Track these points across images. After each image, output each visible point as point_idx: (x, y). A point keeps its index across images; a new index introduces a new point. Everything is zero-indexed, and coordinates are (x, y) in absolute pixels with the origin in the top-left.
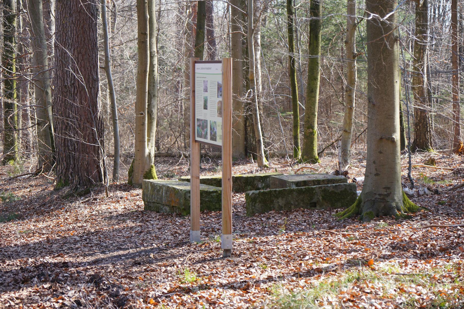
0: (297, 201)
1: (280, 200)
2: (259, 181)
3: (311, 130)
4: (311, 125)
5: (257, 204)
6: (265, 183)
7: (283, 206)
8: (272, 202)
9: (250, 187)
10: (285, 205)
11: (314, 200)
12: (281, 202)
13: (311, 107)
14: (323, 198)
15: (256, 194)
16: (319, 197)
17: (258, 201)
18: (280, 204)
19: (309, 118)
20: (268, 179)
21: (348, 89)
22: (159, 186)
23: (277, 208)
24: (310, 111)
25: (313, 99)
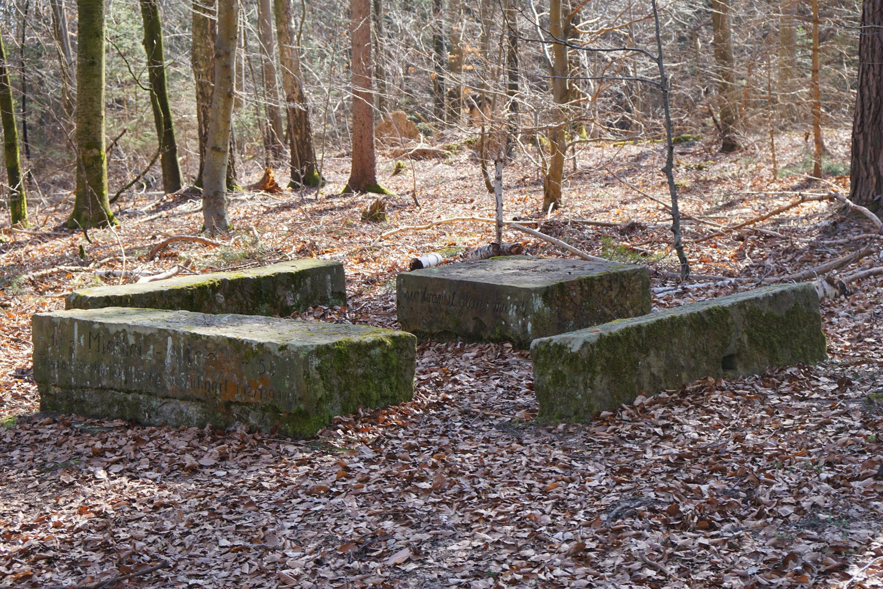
0: (693, 357)
1: (652, 358)
2: (288, 287)
3: (95, 151)
4: (95, 139)
5: (598, 378)
6: (302, 293)
7: (662, 374)
8: (634, 365)
9: (266, 305)
10: (666, 373)
11: (732, 349)
12: (655, 363)
13: (91, 100)
14: (752, 340)
15: (592, 346)
16: (740, 337)
17: (599, 368)
18: (654, 370)
19: (89, 123)
20: (308, 281)
21: (222, 52)
22: (137, 335)
23: (647, 387)
24: (90, 108)
25: (96, 80)
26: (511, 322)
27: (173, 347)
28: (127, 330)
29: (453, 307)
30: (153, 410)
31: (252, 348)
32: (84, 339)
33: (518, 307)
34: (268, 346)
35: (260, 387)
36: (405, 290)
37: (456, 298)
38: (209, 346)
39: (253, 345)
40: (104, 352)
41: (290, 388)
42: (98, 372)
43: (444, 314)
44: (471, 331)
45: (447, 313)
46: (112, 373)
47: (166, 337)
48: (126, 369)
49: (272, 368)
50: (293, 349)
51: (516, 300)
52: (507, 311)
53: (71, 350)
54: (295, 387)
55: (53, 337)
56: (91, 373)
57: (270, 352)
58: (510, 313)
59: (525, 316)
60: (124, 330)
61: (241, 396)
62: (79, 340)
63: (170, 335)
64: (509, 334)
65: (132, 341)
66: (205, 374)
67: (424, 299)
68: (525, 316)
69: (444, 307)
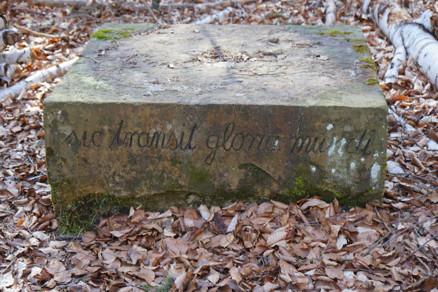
26: (333, 165)
29: (189, 152)
33: (350, 140)
37: (198, 136)
43: (167, 164)
44: (234, 187)
45: (174, 161)
51: (348, 128)
52: (323, 148)
64: (327, 186)
67: (116, 141)
68: (365, 152)
69: (167, 152)
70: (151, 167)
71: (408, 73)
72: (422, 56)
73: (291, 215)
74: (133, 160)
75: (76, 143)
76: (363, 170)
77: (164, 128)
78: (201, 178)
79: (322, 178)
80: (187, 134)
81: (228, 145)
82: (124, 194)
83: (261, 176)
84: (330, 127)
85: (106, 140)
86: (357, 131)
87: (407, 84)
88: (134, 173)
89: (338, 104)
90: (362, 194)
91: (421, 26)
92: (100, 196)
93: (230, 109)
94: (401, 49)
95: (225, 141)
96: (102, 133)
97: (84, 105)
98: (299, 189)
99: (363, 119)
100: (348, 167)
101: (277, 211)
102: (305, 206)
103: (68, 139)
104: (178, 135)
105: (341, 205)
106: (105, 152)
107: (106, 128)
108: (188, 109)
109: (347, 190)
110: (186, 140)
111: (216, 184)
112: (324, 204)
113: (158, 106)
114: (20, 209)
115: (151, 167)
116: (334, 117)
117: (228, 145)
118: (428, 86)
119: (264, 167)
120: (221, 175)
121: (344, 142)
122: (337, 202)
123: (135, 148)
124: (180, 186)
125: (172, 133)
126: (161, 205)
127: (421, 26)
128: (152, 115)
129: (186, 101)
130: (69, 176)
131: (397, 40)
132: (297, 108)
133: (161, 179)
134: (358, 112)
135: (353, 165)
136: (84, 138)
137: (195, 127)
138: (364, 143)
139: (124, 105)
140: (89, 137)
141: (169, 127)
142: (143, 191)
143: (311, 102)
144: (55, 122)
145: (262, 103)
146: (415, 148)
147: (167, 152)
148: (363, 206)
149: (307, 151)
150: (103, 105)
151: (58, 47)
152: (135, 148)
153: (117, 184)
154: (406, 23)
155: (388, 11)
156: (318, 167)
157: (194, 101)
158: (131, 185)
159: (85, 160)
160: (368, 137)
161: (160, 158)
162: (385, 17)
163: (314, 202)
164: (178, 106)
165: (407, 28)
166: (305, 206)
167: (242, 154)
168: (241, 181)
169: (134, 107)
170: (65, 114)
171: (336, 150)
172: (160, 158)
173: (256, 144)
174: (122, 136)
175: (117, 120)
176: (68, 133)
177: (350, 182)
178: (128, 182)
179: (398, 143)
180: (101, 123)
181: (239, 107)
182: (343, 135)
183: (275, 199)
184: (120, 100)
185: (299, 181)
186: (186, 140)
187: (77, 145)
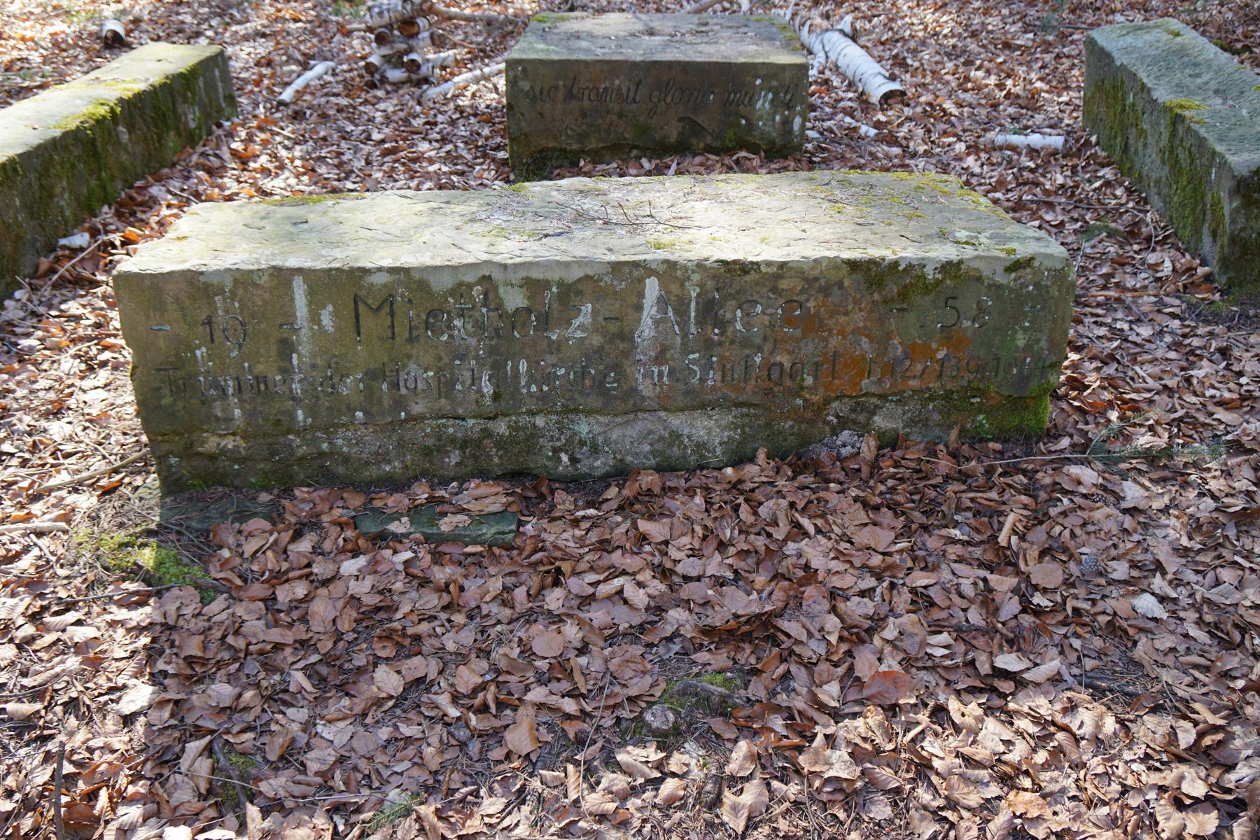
26: (760, 118)
27: (662, 302)
28: (497, 275)
29: (634, 106)
30: (582, 443)
31: (924, 276)
32: (335, 314)
33: (776, 94)
34: (975, 265)
35: (940, 355)
36: (525, 85)
37: (643, 90)
38: (783, 284)
39: (929, 271)
40: (411, 340)
41: (1028, 348)
42: (395, 385)
43: (614, 118)
44: (673, 139)
45: (621, 115)
46: (446, 386)
47: (641, 281)
48: (497, 367)
49: (981, 310)
50: (1048, 264)
51: (774, 83)
52: (752, 102)
53: (286, 348)
54: (1043, 344)
55: (209, 322)
56: (370, 394)
57: (979, 279)
58: (759, 105)
59: (789, 106)
60: (486, 279)
61: (880, 381)
62: (315, 318)
63: (651, 272)
64: (755, 138)
65: (514, 300)
66: (768, 347)
67: (570, 96)
68: (789, 106)
69: (615, 107)
70: (600, 121)
71: (827, 72)
72: (841, 57)
73: (723, 165)
74: (584, 114)
75: (533, 97)
76: (787, 122)
77: (612, 83)
78: (644, 130)
79: (750, 130)
80: (633, 88)
81: (669, 99)
82: (575, 146)
83: (696, 129)
84: (758, 82)
85: (561, 95)
86: (782, 86)
87: (826, 82)
88: (584, 127)
89: (766, 61)
90: (785, 146)
91: (842, 31)
92: (553, 149)
93: (670, 65)
94: (822, 54)
95: (666, 95)
96: (557, 88)
97: (542, 62)
98: (730, 141)
99: (788, 74)
100: (774, 120)
101: (710, 162)
102: (735, 158)
103: (527, 95)
104: (624, 90)
105: (766, 157)
106: (559, 106)
107: (561, 83)
108: (634, 65)
109: (772, 142)
110: (631, 94)
111: (657, 136)
112: (752, 156)
113: (609, 62)
114: (478, 168)
115: (600, 121)
116: (763, 72)
117: (669, 99)
118: (846, 83)
119: (700, 120)
120: (662, 128)
121: (770, 96)
122: (763, 154)
123: (586, 103)
124: (625, 139)
125: (619, 88)
126: (607, 158)
127: (842, 31)
128: (602, 71)
129: (633, 58)
130: (526, 130)
131: (817, 48)
132: (730, 64)
133: (608, 132)
134: (783, 68)
135: (778, 118)
136: (541, 93)
137: (640, 82)
138: (788, 97)
139: (578, 62)
140: (545, 92)
141: (617, 82)
142: (592, 144)
143: (742, 60)
144: (516, 77)
145: (699, 60)
146: (833, 122)
147: (615, 107)
148: (786, 158)
149: (738, 105)
150: (559, 62)
151: (476, 57)
152: (586, 103)
153: (569, 137)
154: (827, 30)
155: (808, 23)
156: (747, 120)
157: (639, 59)
158: (582, 137)
159: (541, 114)
160: (791, 91)
161: (608, 112)
162: (806, 28)
163: (743, 154)
164: (626, 62)
165: (828, 35)
166: (735, 158)
167: (681, 108)
168: (680, 134)
169: (586, 63)
170: (524, 70)
171: (763, 104)
172: (608, 112)
173: (693, 98)
174: (575, 91)
175: (571, 76)
176: (527, 88)
177: (774, 134)
178: (579, 135)
179: (816, 119)
180: (557, 79)
181: (679, 63)
182: (770, 89)
183: (709, 152)
184: (574, 57)
185: (730, 134)
186: (631, 94)
187: (534, 100)
